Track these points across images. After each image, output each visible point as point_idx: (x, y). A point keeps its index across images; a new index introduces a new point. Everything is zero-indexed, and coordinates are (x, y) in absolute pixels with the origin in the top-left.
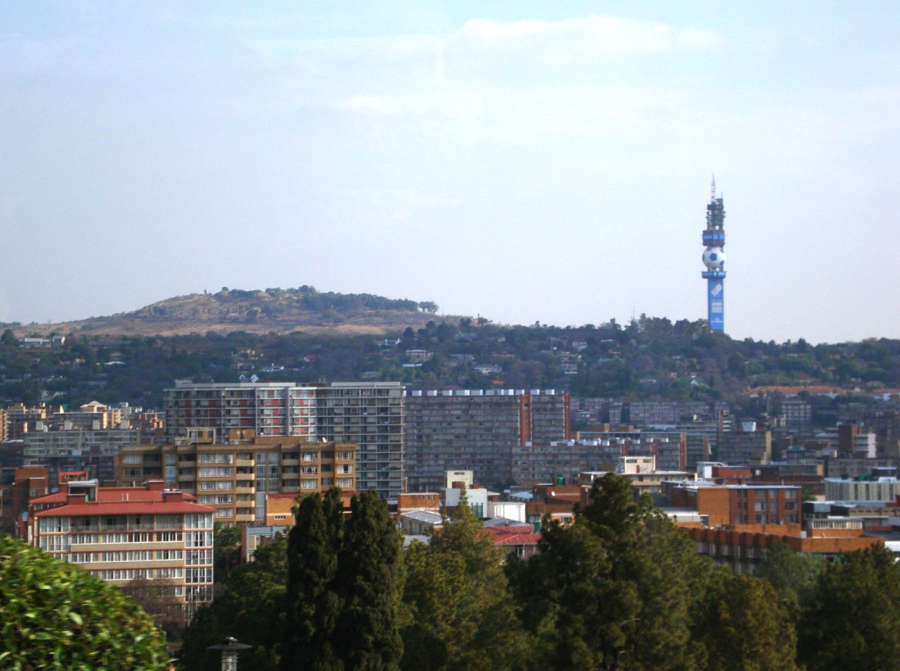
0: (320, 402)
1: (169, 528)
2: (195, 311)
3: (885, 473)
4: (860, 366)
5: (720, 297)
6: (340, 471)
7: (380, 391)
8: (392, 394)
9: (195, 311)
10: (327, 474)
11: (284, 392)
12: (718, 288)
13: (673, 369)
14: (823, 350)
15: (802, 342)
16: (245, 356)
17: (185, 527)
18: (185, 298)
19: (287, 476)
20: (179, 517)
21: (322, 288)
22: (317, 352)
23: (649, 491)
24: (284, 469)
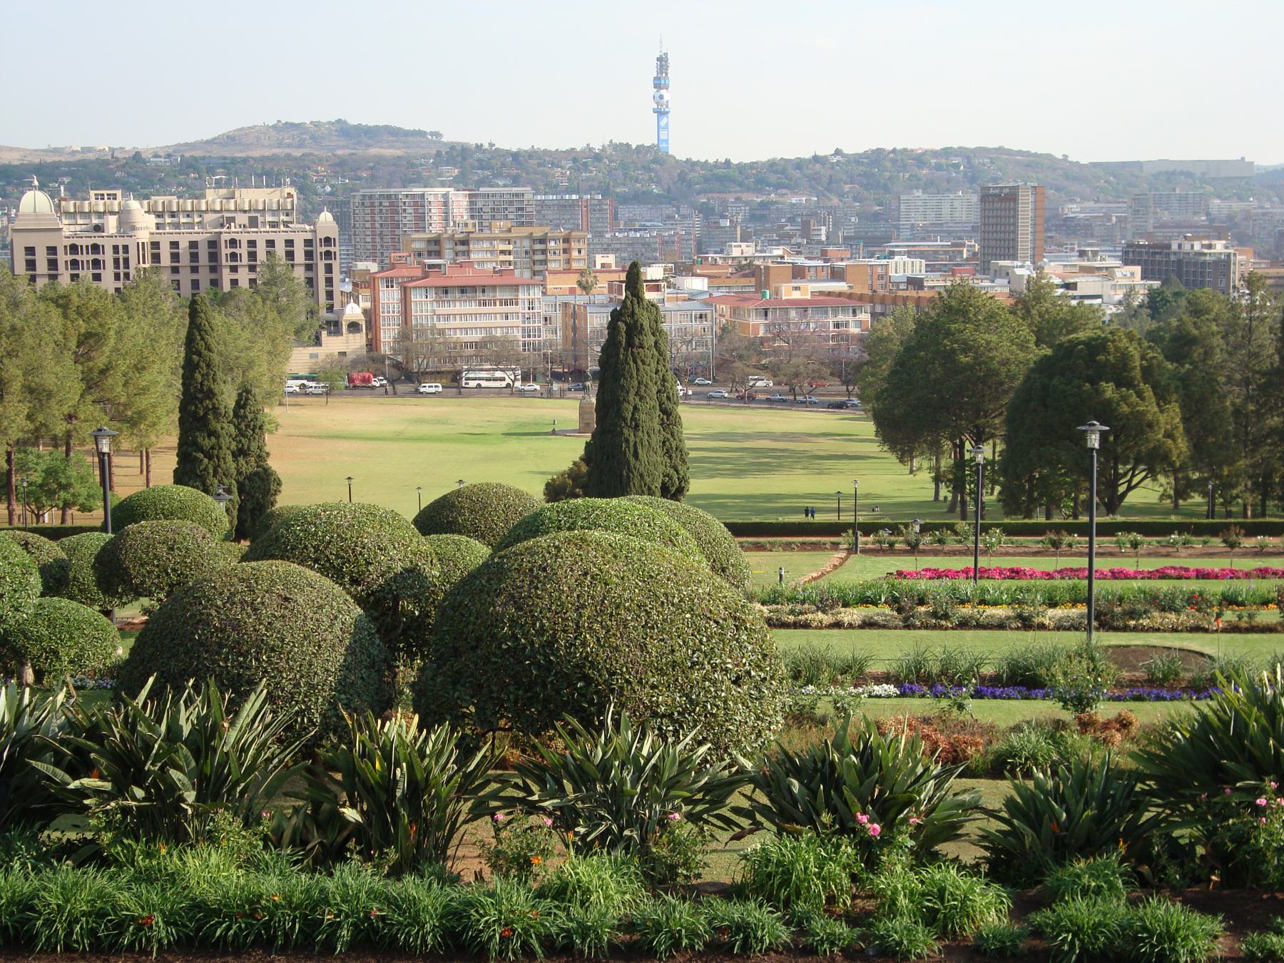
0: (471, 203)
1: (507, 296)
2: (258, 138)
3: (900, 253)
4: (772, 178)
5: (666, 127)
6: (575, 254)
7: (517, 195)
8: (526, 197)
9: (258, 138)
10: (566, 256)
11: (446, 196)
12: (664, 120)
13: (637, 181)
14: (741, 168)
15: (728, 162)
16: (317, 172)
17: (521, 296)
18: (249, 128)
19: (537, 257)
20: (515, 287)
21: (353, 121)
22: (372, 168)
23: (1208, 258)
24: (534, 252)
